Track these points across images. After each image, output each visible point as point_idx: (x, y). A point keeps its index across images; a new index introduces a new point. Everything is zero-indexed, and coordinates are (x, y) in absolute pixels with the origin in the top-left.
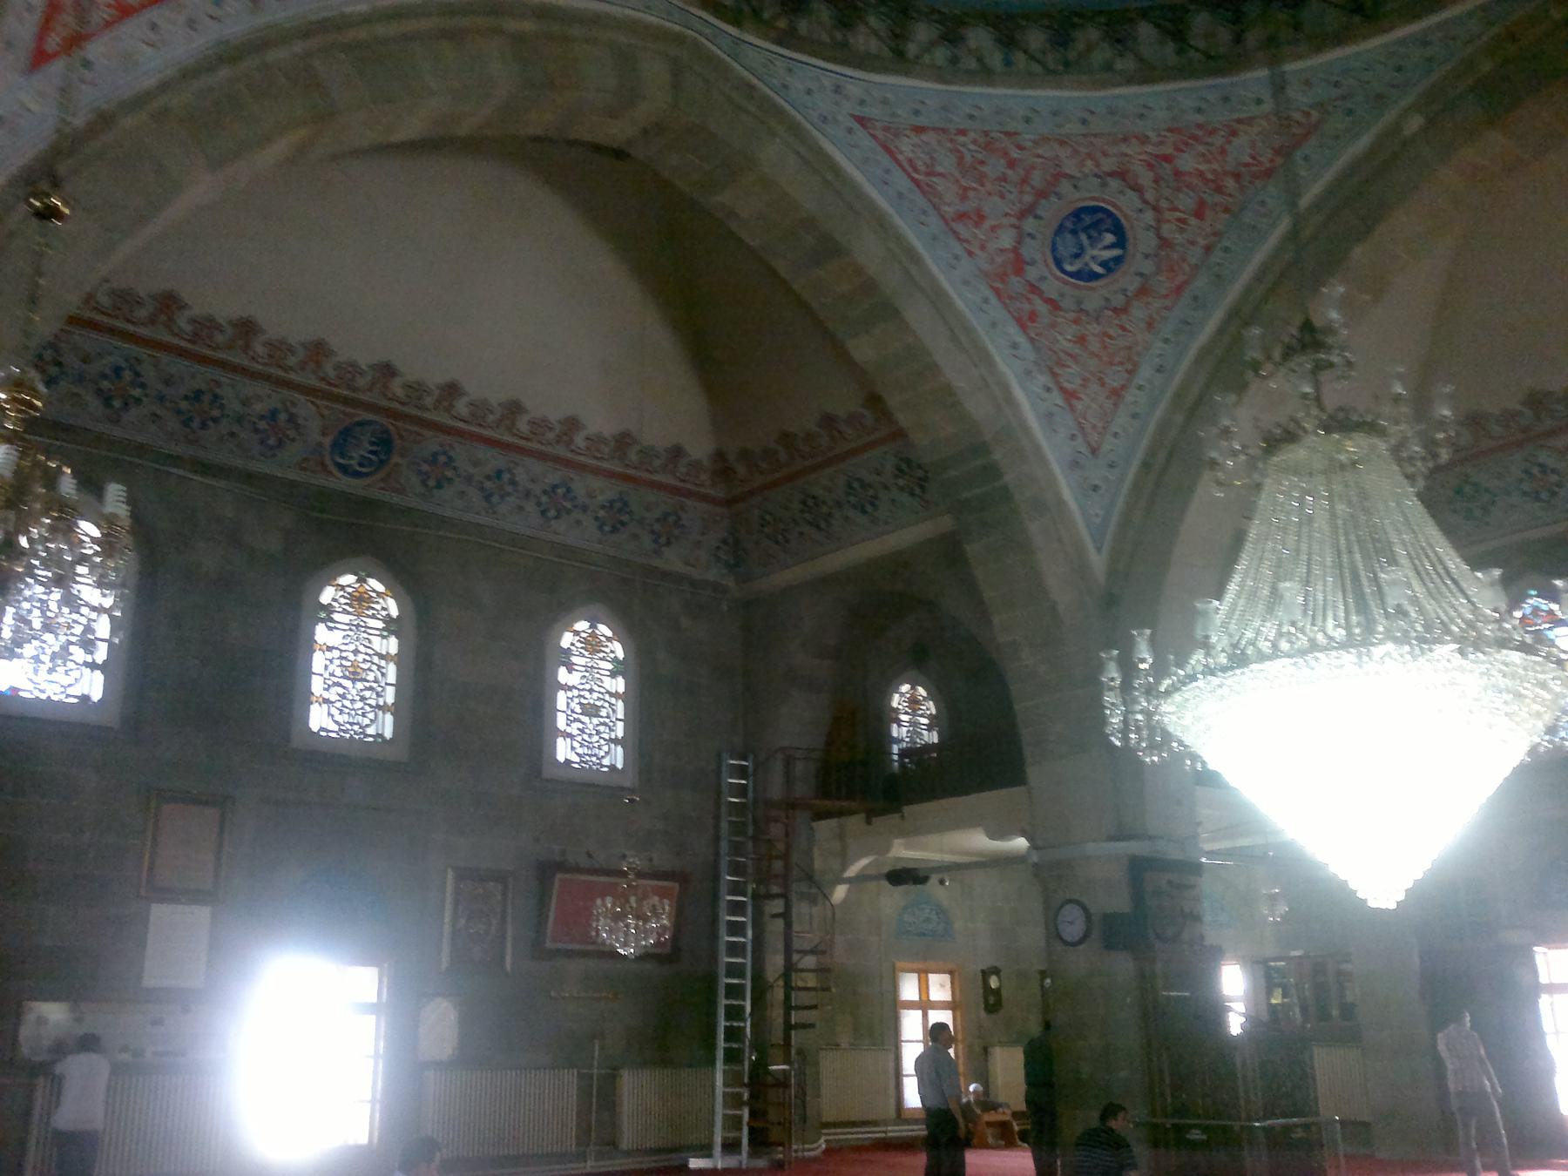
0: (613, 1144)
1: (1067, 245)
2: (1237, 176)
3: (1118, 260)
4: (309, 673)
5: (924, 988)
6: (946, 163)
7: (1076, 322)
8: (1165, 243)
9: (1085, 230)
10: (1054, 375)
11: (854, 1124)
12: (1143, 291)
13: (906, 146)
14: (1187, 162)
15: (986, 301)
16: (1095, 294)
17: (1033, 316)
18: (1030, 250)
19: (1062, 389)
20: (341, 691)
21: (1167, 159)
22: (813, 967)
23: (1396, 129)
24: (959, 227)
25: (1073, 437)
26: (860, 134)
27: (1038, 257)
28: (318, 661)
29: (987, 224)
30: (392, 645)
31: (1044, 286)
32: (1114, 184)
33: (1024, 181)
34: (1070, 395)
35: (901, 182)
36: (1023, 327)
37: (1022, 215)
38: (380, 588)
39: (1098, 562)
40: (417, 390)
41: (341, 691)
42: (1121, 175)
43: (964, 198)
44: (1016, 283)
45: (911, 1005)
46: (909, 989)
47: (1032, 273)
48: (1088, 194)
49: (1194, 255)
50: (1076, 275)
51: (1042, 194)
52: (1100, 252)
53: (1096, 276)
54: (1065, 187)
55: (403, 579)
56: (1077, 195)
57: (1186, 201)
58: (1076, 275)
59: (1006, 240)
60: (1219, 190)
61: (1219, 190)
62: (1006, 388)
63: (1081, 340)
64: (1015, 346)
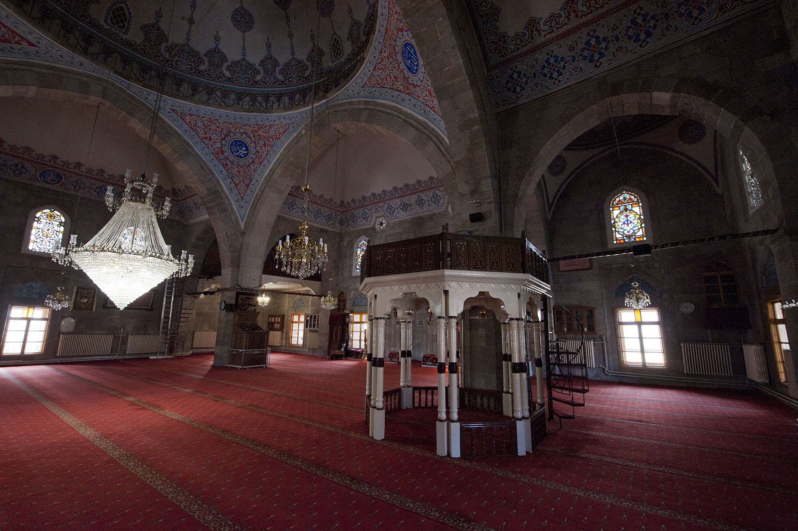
0: (125, 353)
1: (234, 149)
2: (272, 138)
3: (247, 154)
4: (30, 234)
5: (361, 318)
6: (200, 124)
7: (238, 167)
8: (257, 151)
9: (239, 145)
10: (233, 180)
11: (210, 348)
12: (253, 162)
13: (188, 118)
14: (260, 133)
15: (213, 159)
16: (242, 162)
17: (227, 165)
18: (225, 149)
19: (235, 183)
20: (42, 239)
21: (256, 132)
22: (41, 317)
23: (300, 133)
24: (204, 140)
25: (237, 195)
26: (172, 113)
27: (227, 150)
28: (33, 232)
29: (213, 141)
30: (62, 229)
31: (229, 157)
32: (244, 135)
33: (222, 131)
34: (236, 185)
35: (187, 127)
36: (224, 167)
37: (222, 140)
38: (59, 214)
39: (242, 225)
40: (66, 163)
41: (42, 239)
42: (246, 133)
43: (205, 134)
44: (221, 156)
45: (296, 322)
46: (296, 318)
47: (226, 154)
48: (238, 137)
49: (264, 155)
50: (237, 156)
51: (226, 135)
52: (243, 151)
53: (243, 157)
54: (232, 134)
55: (64, 210)
56: (235, 137)
57: (262, 143)
58: (237, 156)
59: (219, 145)
60: (269, 141)
61: (269, 141)
62: (218, 181)
63: (239, 172)
64: (221, 171)
